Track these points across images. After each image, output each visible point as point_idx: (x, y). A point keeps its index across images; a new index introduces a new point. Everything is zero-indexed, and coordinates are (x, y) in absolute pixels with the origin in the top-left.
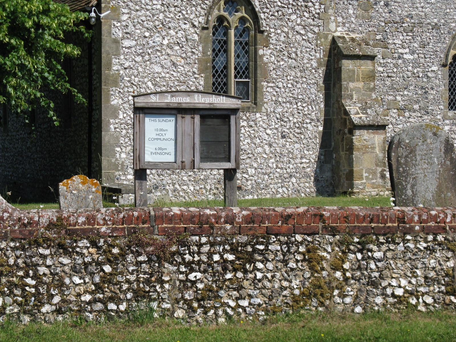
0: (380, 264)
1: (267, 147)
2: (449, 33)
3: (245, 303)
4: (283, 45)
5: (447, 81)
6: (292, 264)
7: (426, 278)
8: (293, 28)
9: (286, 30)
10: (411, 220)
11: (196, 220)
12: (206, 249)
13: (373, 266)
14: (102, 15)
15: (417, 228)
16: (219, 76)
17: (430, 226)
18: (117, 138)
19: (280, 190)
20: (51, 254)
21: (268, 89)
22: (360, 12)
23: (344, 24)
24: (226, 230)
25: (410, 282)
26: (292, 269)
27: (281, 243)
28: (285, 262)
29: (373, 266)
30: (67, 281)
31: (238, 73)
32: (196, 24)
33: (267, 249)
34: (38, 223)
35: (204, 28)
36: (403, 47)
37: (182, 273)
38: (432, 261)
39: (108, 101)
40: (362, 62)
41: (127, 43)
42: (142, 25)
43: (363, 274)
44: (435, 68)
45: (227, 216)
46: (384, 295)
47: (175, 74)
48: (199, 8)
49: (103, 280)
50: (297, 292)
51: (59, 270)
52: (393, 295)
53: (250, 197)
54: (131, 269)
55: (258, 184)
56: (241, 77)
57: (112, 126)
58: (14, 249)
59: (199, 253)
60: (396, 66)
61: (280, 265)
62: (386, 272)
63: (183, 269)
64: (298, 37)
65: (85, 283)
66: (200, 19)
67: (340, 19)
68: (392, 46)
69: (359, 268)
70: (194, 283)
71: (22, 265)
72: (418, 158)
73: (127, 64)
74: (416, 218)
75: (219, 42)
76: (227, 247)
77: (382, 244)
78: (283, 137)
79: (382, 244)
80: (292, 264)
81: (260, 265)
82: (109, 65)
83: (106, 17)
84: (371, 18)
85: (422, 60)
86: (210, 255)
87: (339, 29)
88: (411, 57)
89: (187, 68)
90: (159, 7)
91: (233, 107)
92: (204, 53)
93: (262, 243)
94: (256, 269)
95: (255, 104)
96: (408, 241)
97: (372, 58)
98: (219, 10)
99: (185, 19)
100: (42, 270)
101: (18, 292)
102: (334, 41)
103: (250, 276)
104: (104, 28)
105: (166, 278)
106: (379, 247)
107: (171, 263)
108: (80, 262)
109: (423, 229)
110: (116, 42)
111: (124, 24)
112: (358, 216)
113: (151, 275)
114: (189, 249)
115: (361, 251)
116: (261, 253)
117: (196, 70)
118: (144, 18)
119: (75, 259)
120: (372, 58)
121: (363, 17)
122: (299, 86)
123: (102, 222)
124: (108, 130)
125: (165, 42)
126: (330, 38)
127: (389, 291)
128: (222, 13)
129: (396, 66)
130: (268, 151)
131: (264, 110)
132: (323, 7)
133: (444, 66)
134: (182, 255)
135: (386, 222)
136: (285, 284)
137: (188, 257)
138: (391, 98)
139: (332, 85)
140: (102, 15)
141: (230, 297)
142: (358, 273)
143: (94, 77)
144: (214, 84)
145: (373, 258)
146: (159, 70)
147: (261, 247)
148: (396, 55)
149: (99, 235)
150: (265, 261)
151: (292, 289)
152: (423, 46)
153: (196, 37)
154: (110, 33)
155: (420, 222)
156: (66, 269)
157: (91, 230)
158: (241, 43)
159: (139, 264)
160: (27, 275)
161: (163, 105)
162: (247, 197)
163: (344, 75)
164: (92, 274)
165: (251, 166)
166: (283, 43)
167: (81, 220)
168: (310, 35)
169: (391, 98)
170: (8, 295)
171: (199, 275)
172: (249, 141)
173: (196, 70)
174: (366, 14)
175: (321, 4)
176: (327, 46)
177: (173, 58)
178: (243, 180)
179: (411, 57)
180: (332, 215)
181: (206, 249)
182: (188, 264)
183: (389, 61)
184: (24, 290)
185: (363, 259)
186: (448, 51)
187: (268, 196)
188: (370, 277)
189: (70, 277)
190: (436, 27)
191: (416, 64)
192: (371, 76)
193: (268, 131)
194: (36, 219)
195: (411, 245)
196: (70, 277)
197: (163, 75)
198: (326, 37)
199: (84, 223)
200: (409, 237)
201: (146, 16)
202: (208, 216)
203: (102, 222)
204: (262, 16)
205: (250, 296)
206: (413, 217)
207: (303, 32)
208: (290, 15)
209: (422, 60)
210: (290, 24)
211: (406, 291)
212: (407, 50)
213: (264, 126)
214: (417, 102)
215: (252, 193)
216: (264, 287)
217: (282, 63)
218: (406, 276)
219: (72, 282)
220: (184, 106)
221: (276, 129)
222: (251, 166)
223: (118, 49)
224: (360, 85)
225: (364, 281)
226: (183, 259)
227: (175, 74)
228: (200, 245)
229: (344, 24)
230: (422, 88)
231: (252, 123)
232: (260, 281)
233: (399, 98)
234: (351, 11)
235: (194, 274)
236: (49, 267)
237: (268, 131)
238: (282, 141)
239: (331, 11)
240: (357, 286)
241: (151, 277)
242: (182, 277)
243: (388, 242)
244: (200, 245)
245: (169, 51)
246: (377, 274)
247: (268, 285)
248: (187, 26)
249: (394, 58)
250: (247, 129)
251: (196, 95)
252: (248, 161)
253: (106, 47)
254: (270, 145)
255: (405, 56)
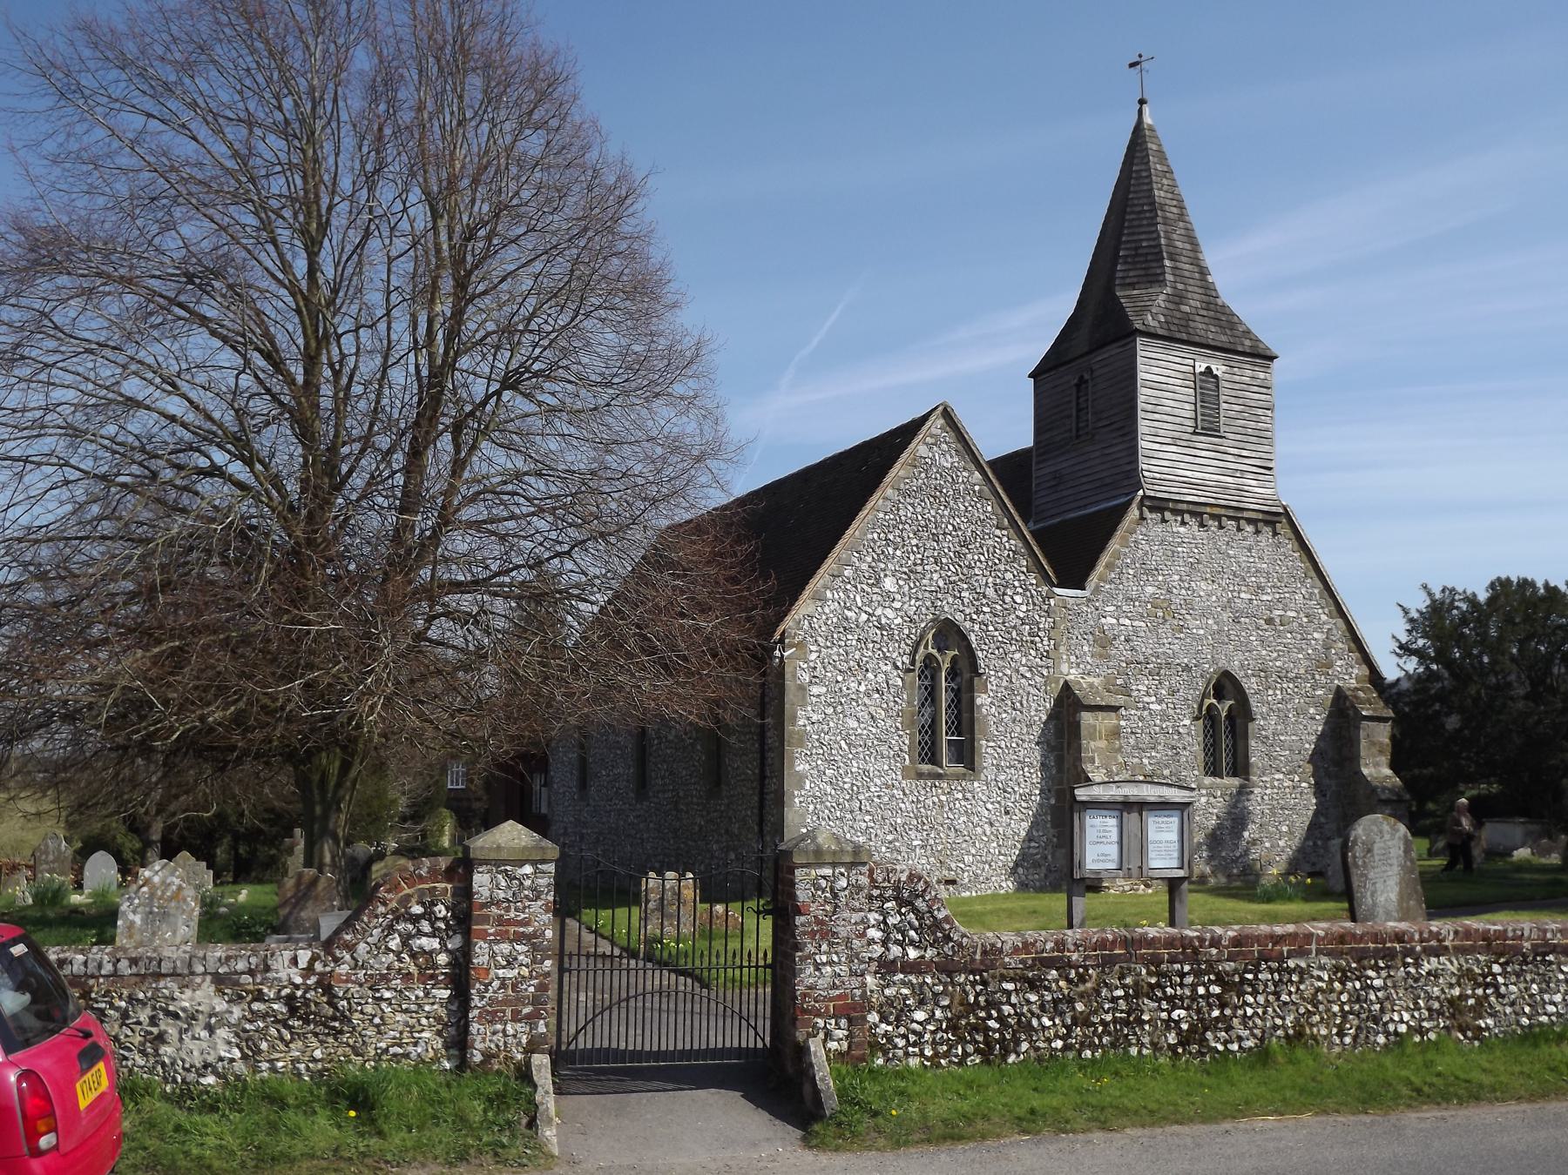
0: (1380, 994)
1: (987, 827)
2: (1202, 676)
3: (1235, 1047)
4: (1005, 693)
5: (1201, 739)
6: (1285, 998)
7: (1429, 1009)
8: (1018, 671)
9: (1008, 672)
10: (1412, 939)
11: (1178, 943)
12: (1189, 980)
13: (1373, 997)
14: (786, 654)
15: (1418, 948)
16: (926, 732)
17: (1432, 947)
18: (803, 816)
19: (1004, 884)
20: (1016, 990)
21: (989, 750)
22: (1098, 649)
23: (1078, 665)
24: (1211, 955)
25: (1413, 1016)
26: (1285, 1003)
27: (1272, 971)
28: (1277, 995)
29: (1373, 997)
30: (1035, 1022)
31: (950, 728)
32: (899, 664)
33: (1256, 978)
34: (1001, 951)
35: (908, 671)
36: (1148, 694)
37: (1163, 1010)
38: (1435, 989)
39: (792, 765)
40: (1105, 714)
41: (815, 690)
42: (835, 667)
43: (1362, 1007)
44: (1187, 722)
45: (1212, 938)
46: (1387, 1034)
47: (874, 730)
48: (903, 645)
49: (1075, 1022)
50: (1291, 1032)
51: (1025, 1009)
52: (1396, 1033)
53: (968, 894)
54: (1106, 1006)
55: (976, 875)
56: (953, 735)
57: (797, 800)
58: (974, 984)
59: (1182, 985)
60: (1141, 718)
61: (1271, 998)
62: (1388, 1005)
63: (1164, 1005)
64: (1023, 681)
65: (1054, 1024)
66: (905, 658)
67: (1073, 659)
68: (1135, 694)
69: (1358, 1000)
70: (1177, 1022)
71: (983, 1004)
72: (1377, 858)
73: (815, 718)
74: (1417, 937)
75: (926, 689)
76: (1212, 977)
77: (1382, 969)
78: (1007, 813)
79: (1382, 969)
80: (1285, 998)
81: (1250, 999)
82: (794, 718)
83: (788, 657)
84: (1108, 657)
85: (1171, 712)
86: (1194, 987)
87: (1072, 671)
88: (1159, 708)
89: (889, 722)
90: (854, 642)
91: (1186, 800)
92: (909, 703)
93: (1250, 972)
94: (1246, 1004)
95: (973, 770)
96: (1409, 964)
97: (1115, 709)
98: (926, 647)
99: (886, 658)
100: (1007, 1009)
101: (980, 1038)
102: (1066, 685)
103: (1240, 1012)
104: (788, 669)
105: (1146, 1017)
106: (1378, 973)
107: (1151, 999)
108: (1049, 998)
109: (1424, 950)
110: (802, 688)
111: (812, 664)
112: (1354, 935)
113: (1129, 1014)
114: (1171, 981)
115: (1358, 979)
116: (1250, 983)
117: (899, 725)
118: (836, 658)
119: (1043, 996)
120: (1115, 709)
121: (1101, 656)
122: (1026, 745)
123: (1072, 948)
124: (792, 805)
125: (862, 688)
126: (1062, 682)
127: (1391, 1027)
128: (930, 650)
129: (1141, 718)
130: (988, 833)
131: (983, 777)
132: (1052, 642)
133: (1197, 719)
134: (1163, 988)
135: (1384, 943)
136: (1279, 1022)
137: (1169, 990)
138: (1136, 760)
139: (1066, 745)
140: (786, 654)
141: (1217, 1040)
142: (1357, 1007)
143: (769, 734)
144: (920, 743)
145: (1372, 987)
146: (856, 725)
147: (1250, 976)
148: (1140, 705)
149: (1070, 965)
150: (1255, 993)
151: (1284, 1027)
152: (1173, 692)
153: (900, 682)
154: (794, 676)
155: (1421, 941)
156: (1034, 1008)
157: (1061, 958)
158: (953, 689)
159: (1114, 1000)
160: (990, 1017)
161: (1105, 799)
162: (963, 894)
163: (1083, 732)
164: (1062, 1014)
165: (968, 853)
166: (1006, 688)
167: (1049, 945)
168: (1038, 679)
169: (1136, 760)
170: (970, 1042)
171: (1183, 1013)
172: (965, 819)
173: (899, 725)
174: (1103, 651)
175: (1049, 639)
176: (1056, 689)
177: (872, 709)
178: (959, 871)
179: (1159, 708)
180: (1327, 934)
181: (1189, 980)
182: (1170, 999)
183: (1133, 712)
184: (986, 1036)
185: (1362, 989)
186: (1202, 701)
187: (989, 892)
188: (1370, 1011)
189: (1039, 1018)
190: (1187, 668)
191: (1165, 716)
192: (1116, 733)
193: (989, 806)
194: (999, 945)
195: (1412, 970)
196: (1039, 1018)
197: (859, 731)
198: (1057, 682)
199: (1053, 950)
200: (1409, 960)
201: (839, 655)
202: (1191, 939)
203: (1072, 948)
204: (979, 654)
205: (1240, 1039)
206: (1413, 935)
207: (1029, 675)
208: (1014, 652)
209: (1171, 712)
210: (1013, 665)
211: (1409, 1027)
212: (1153, 699)
213: (984, 798)
214: (1167, 766)
215: (969, 889)
216: (1256, 1026)
217: (1004, 715)
218: (1407, 1009)
219: (1040, 1023)
220: (1132, 799)
221: (999, 803)
222: (968, 853)
223: (804, 697)
224: (1102, 744)
225: (1364, 1016)
226: (1164, 993)
227: (874, 730)
228: (1182, 975)
229: (1078, 665)
230: (1173, 748)
231: (969, 795)
232: (1250, 1018)
233: (1146, 761)
234: (1086, 648)
235: (1177, 1012)
236: (1013, 1006)
237: (989, 806)
238: (1005, 818)
239: (1062, 649)
240: (1356, 1022)
241: (1129, 1016)
242: (1164, 1015)
243: (1388, 967)
244: (1182, 975)
245: (866, 700)
246: (1377, 1007)
247: (1258, 1021)
248: (889, 668)
249: (1138, 709)
250: (963, 803)
251: (1145, 786)
252: (964, 845)
253: (790, 696)
254: (991, 825)
255: (1151, 706)
